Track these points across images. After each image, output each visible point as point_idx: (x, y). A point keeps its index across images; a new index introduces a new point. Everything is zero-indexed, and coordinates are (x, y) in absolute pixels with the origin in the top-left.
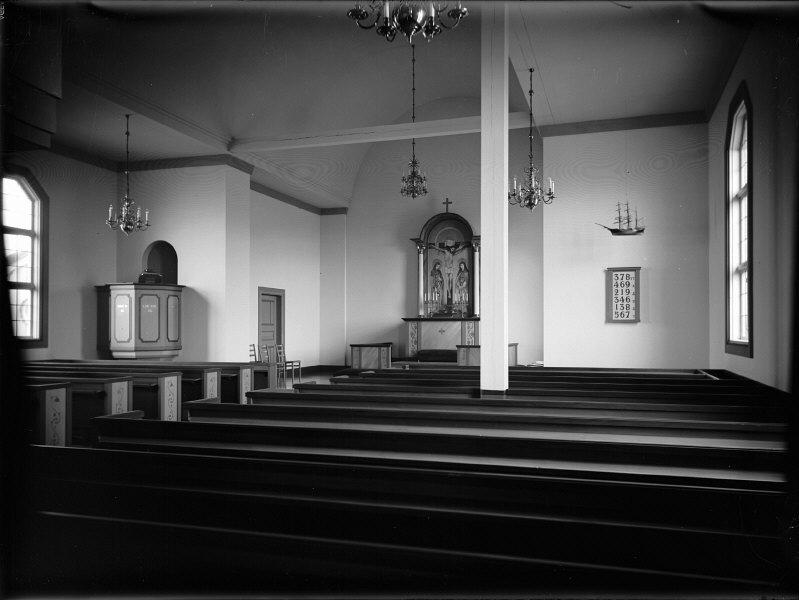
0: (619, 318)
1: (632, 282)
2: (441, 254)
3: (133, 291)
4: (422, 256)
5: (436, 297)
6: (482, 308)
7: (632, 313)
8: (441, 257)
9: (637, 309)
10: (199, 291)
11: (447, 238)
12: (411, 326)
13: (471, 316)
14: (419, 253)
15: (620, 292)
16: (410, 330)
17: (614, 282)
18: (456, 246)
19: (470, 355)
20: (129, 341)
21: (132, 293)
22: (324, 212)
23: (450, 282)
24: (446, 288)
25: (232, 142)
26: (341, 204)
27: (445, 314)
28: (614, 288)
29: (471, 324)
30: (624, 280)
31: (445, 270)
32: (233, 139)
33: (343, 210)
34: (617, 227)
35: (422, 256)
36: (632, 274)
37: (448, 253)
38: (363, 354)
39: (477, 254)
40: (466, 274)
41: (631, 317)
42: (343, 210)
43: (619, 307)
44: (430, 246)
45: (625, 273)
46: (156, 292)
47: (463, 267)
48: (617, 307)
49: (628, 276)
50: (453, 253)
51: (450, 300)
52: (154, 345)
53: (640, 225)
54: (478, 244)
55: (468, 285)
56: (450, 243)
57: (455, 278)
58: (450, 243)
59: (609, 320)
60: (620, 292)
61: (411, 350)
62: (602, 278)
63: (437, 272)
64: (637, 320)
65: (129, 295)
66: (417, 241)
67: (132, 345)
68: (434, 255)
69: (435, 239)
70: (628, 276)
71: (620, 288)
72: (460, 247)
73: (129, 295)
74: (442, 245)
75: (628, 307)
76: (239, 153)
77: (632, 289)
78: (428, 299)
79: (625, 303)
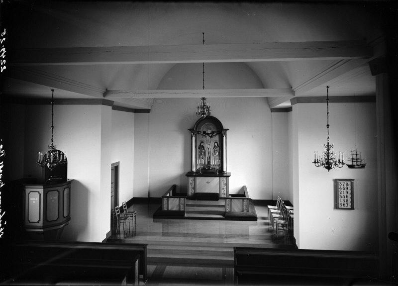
0: (343, 207)
1: (349, 187)
2: (204, 137)
3: (42, 190)
4: (194, 138)
5: (203, 161)
6: (228, 168)
7: (350, 204)
8: (204, 139)
9: (352, 202)
10: (81, 182)
11: (208, 129)
12: (191, 179)
13: (220, 173)
14: (192, 137)
15: (343, 192)
16: (190, 181)
17: (340, 187)
18: (213, 133)
19: (233, 204)
20: (38, 222)
21: (41, 191)
22: (136, 111)
23: (209, 153)
24: (207, 156)
25: (105, 94)
26: (149, 108)
27: (207, 172)
28: (340, 190)
29: (225, 179)
30: (345, 186)
31: (206, 146)
32: (107, 90)
33: (148, 111)
34: (350, 163)
35: (194, 138)
36: (349, 183)
37: (208, 137)
38: (169, 202)
39: (224, 138)
40: (218, 148)
41: (349, 207)
42: (148, 111)
43: (342, 201)
44: (199, 133)
45: (345, 182)
46: (57, 188)
47: (216, 144)
48: (341, 201)
49: (347, 184)
50: (211, 137)
51: (209, 163)
52: (56, 222)
53: (363, 162)
54: (225, 133)
55: (219, 154)
56: (209, 131)
57: (212, 151)
58: (209, 131)
59: (336, 207)
60: (343, 192)
61: (190, 192)
62: (332, 183)
63: (201, 147)
64: (352, 208)
65: (39, 192)
66: (191, 130)
67: (41, 224)
68: (200, 138)
69: (202, 129)
70: (347, 184)
71: (342, 190)
72: (215, 134)
73: (39, 192)
74: (204, 132)
75: (347, 201)
76: (108, 98)
77: (349, 191)
78: (197, 164)
79: (346, 199)
